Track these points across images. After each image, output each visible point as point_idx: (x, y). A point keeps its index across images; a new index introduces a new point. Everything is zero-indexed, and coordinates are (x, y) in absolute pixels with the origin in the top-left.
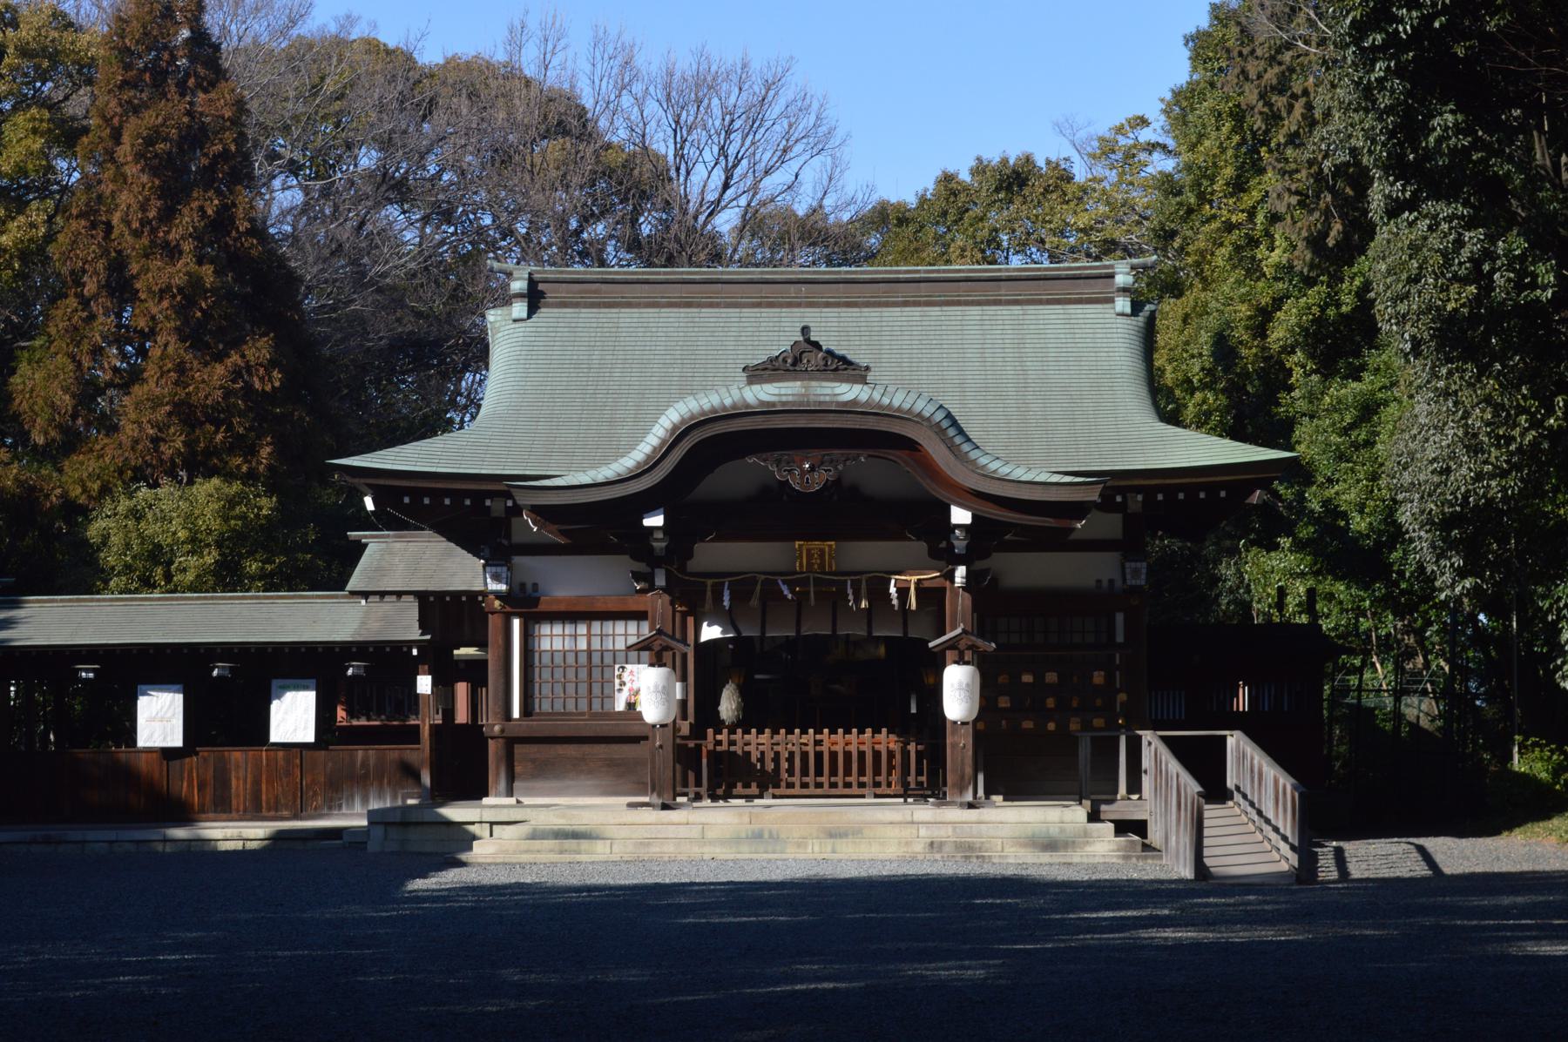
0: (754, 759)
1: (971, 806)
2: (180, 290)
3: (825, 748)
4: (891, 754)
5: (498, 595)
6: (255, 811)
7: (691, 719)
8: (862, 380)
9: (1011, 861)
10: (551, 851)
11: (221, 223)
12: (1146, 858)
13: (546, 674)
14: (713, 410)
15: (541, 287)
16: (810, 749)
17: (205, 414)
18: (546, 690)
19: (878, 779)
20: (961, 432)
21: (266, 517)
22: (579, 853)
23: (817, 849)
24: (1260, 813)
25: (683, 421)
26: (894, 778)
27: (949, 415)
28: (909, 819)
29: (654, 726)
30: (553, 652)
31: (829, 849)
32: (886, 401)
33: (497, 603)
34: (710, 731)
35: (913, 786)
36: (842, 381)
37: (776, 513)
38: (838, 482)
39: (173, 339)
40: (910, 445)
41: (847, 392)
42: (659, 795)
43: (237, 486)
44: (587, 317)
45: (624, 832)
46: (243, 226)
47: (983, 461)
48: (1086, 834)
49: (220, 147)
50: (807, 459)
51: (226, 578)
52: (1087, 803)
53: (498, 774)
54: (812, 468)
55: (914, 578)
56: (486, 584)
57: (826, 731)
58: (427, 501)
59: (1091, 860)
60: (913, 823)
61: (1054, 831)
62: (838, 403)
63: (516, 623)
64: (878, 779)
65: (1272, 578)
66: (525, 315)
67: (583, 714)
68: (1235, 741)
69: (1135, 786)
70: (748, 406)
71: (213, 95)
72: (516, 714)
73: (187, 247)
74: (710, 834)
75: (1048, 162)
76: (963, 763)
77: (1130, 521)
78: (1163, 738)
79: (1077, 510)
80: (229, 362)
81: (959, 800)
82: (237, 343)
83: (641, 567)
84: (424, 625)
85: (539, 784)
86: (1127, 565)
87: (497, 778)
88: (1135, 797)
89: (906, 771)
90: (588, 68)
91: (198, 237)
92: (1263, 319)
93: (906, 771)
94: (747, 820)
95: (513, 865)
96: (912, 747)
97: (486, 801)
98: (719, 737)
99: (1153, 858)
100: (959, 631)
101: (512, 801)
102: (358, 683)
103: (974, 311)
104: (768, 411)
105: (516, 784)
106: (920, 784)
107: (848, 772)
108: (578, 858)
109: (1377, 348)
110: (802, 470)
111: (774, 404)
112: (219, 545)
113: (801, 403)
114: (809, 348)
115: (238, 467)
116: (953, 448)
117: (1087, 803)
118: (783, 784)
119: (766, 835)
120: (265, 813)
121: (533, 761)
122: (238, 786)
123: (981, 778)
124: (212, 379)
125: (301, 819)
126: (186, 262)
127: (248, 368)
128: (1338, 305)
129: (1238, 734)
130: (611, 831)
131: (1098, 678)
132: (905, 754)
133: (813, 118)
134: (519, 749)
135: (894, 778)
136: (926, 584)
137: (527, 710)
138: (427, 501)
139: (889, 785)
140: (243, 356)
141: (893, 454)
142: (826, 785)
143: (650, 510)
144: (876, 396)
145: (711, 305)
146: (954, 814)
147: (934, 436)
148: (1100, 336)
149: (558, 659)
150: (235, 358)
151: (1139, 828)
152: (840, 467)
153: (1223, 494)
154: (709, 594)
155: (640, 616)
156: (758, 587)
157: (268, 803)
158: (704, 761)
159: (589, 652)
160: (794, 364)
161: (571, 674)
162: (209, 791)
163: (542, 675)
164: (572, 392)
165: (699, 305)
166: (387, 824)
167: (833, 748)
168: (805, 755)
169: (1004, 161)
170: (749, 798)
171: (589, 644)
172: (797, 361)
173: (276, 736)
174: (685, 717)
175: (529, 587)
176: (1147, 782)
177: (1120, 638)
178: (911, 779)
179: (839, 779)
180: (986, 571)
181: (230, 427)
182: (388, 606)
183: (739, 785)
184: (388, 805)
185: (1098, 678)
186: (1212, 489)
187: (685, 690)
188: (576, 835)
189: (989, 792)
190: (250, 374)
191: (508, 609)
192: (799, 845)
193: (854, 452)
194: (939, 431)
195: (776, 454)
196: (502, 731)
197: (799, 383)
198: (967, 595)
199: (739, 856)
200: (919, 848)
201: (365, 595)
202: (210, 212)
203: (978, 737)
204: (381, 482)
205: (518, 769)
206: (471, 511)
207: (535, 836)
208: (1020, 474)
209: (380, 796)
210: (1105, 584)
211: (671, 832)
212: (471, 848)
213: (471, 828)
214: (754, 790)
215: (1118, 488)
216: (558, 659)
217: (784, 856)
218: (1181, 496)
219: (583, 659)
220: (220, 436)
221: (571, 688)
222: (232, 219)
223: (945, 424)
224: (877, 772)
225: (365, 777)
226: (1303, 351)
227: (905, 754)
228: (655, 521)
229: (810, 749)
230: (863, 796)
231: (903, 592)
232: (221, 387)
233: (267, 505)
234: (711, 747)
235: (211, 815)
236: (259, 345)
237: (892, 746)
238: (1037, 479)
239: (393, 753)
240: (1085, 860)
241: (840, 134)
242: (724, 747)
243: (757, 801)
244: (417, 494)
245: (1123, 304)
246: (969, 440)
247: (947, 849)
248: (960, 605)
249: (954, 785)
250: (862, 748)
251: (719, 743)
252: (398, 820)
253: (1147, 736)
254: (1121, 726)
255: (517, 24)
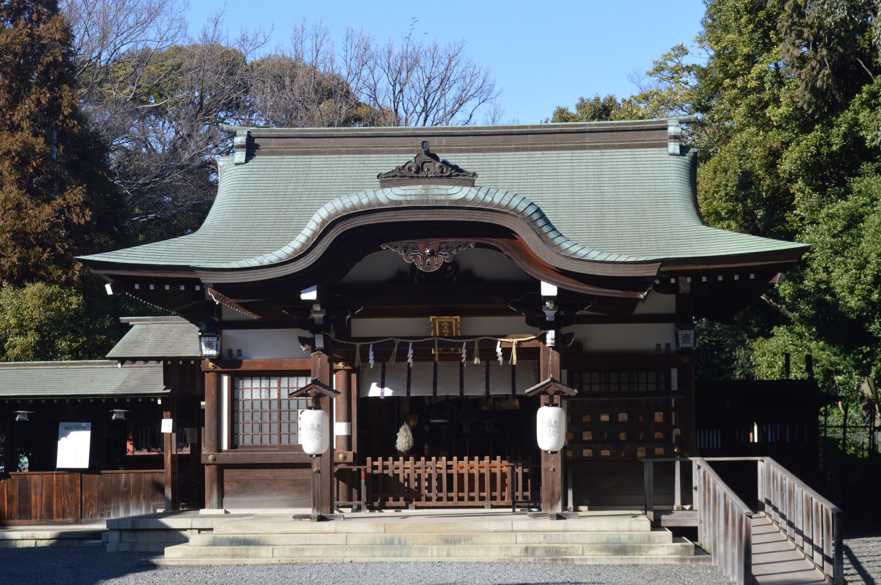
0: (401, 480)
1: (559, 517)
2: (18, 154)
3: (454, 471)
4: (504, 476)
5: (212, 359)
6: (48, 518)
7: (355, 450)
8: (472, 184)
9: (589, 563)
10: (226, 555)
11: (53, 108)
12: (698, 560)
13: (248, 417)
14: (353, 208)
15: (256, 141)
16: (443, 472)
17: (37, 239)
18: (248, 429)
19: (494, 494)
20: (548, 223)
21: (74, 310)
22: (247, 557)
23: (435, 553)
24: (791, 524)
25: (330, 216)
26: (506, 493)
27: (538, 210)
28: (510, 528)
29: (311, 456)
30: (252, 401)
31: (445, 553)
32: (488, 199)
33: (211, 364)
34: (369, 459)
35: (520, 499)
36: (455, 184)
37: (410, 293)
38: (454, 264)
39: (14, 188)
40: (508, 234)
41: (457, 192)
42: (318, 510)
43: (56, 289)
44: (288, 161)
45: (285, 540)
46: (67, 111)
47: (565, 245)
48: (650, 540)
49: (51, 58)
50: (428, 246)
51: (44, 351)
52: (651, 514)
53: (211, 492)
54: (432, 253)
55: (515, 341)
56: (201, 350)
57: (455, 458)
58: (152, 287)
59: (654, 563)
60: (512, 531)
61: (624, 537)
62: (451, 201)
63: (225, 379)
64: (494, 494)
65: (773, 355)
66: (243, 160)
67: (274, 446)
68: (765, 466)
69: (687, 498)
70: (380, 204)
71: (49, 25)
72: (225, 447)
73: (25, 125)
74: (353, 541)
75: (624, 101)
76: (553, 484)
77: (681, 300)
78: (709, 463)
79: (639, 283)
80: (54, 203)
81: (550, 512)
82: (61, 191)
83: (307, 334)
84: (167, 383)
85: (242, 499)
86: (680, 332)
87: (211, 496)
88: (687, 507)
89: (514, 488)
90: (343, 53)
91: (32, 118)
92: (774, 156)
93: (514, 488)
94: (382, 529)
95: (193, 567)
96: (519, 470)
97: (202, 512)
98: (375, 463)
99: (704, 560)
100: (549, 380)
101: (221, 512)
102: (118, 425)
103: (567, 154)
104: (397, 208)
105: (225, 499)
106: (525, 498)
107: (472, 489)
108: (245, 561)
109: (860, 176)
110: (424, 254)
111: (400, 202)
112: (38, 330)
113: (422, 201)
114: (429, 159)
115: (59, 277)
116: (541, 235)
117: (651, 514)
118: (423, 498)
119: (396, 542)
120: (55, 520)
121: (238, 482)
122: (37, 500)
123: (570, 493)
124: (42, 215)
125: (81, 524)
126: (25, 135)
127: (69, 208)
128: (830, 145)
129: (768, 459)
130: (274, 539)
131: (659, 417)
132: (514, 475)
133: (481, 81)
134: (227, 473)
135: (506, 493)
136: (525, 345)
137: (233, 445)
138: (152, 287)
139: (503, 498)
140: (65, 199)
141: (495, 242)
142: (455, 499)
143: (306, 286)
144: (481, 195)
145: (377, 152)
146: (546, 524)
147: (525, 225)
148: (664, 166)
149: (257, 406)
150: (60, 200)
151: (691, 533)
152: (454, 252)
153: (752, 276)
154: (358, 353)
155: (306, 373)
156: (396, 349)
157: (57, 512)
158: (363, 481)
159: (279, 401)
160: (417, 172)
161: (266, 417)
162: (16, 504)
163: (245, 418)
164: (262, 213)
165: (369, 153)
166: (121, 530)
167: (461, 471)
168: (440, 477)
169: (597, 100)
170: (398, 508)
171: (279, 394)
172: (419, 169)
173: (60, 464)
174: (349, 448)
175: (235, 353)
176: (697, 496)
177: (675, 387)
178: (519, 494)
179: (465, 494)
180: (571, 335)
181: (54, 249)
182: (140, 369)
183: (391, 499)
184: (144, 513)
185: (659, 417)
186: (744, 272)
187: (350, 428)
188: (247, 543)
189: (577, 504)
190: (69, 211)
191: (219, 369)
192: (421, 550)
193: (465, 240)
194: (532, 222)
195: (404, 242)
196: (214, 459)
197: (421, 186)
198: (555, 352)
199: (373, 559)
200: (516, 551)
201: (122, 360)
202: (44, 102)
203: (567, 463)
204: (116, 273)
205: (227, 488)
206: (177, 294)
207: (215, 543)
208: (595, 255)
209: (138, 506)
210: (663, 347)
211: (321, 539)
212: (163, 553)
213: (184, 533)
214: (402, 502)
215: (672, 273)
216: (257, 406)
217: (408, 559)
218: (720, 278)
219: (275, 406)
220: (46, 255)
221: (266, 428)
222: (59, 107)
223: (535, 217)
224: (493, 489)
225: (127, 493)
226: (804, 181)
227: (514, 475)
228: (310, 295)
229: (443, 472)
230: (483, 507)
231: (507, 352)
232: (48, 221)
233: (75, 301)
234: (369, 471)
235: (17, 521)
236: (75, 192)
237: (505, 469)
238: (608, 259)
239: (148, 475)
240: (649, 562)
241: (496, 90)
242: (379, 471)
243: (404, 512)
244: (145, 282)
245: (674, 147)
246: (554, 229)
247: (538, 553)
248: (551, 360)
249: (547, 501)
250: (482, 471)
251: (376, 468)
252: (129, 527)
253: (696, 461)
254: (676, 454)
255: (299, 27)
